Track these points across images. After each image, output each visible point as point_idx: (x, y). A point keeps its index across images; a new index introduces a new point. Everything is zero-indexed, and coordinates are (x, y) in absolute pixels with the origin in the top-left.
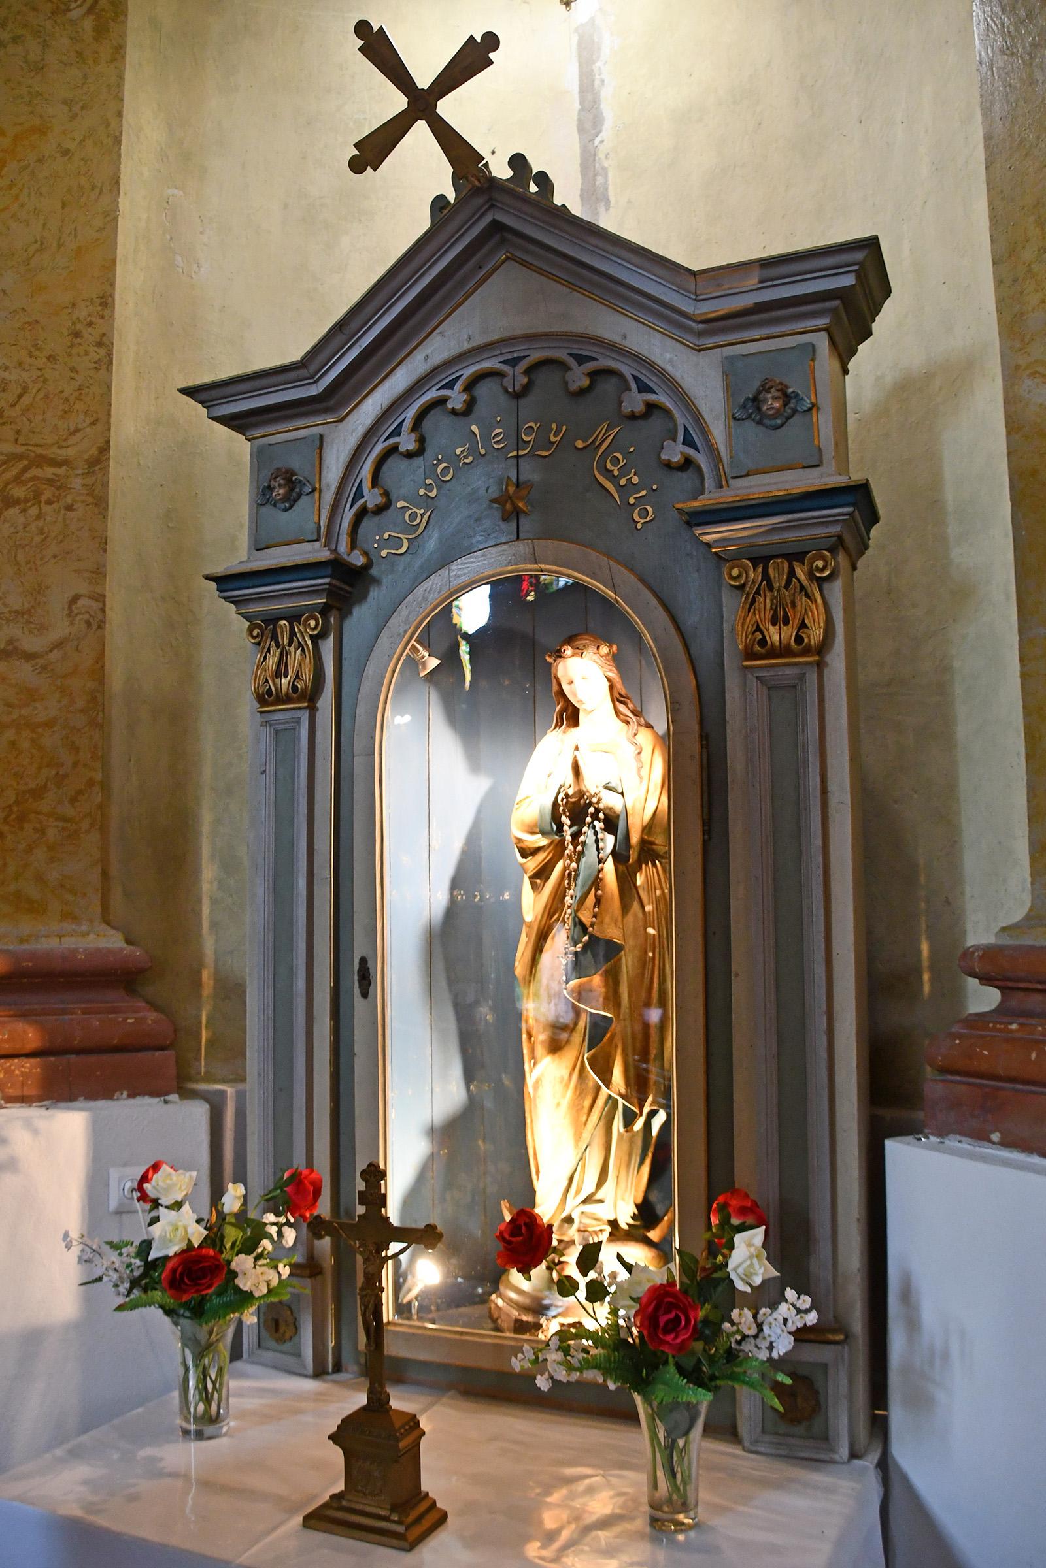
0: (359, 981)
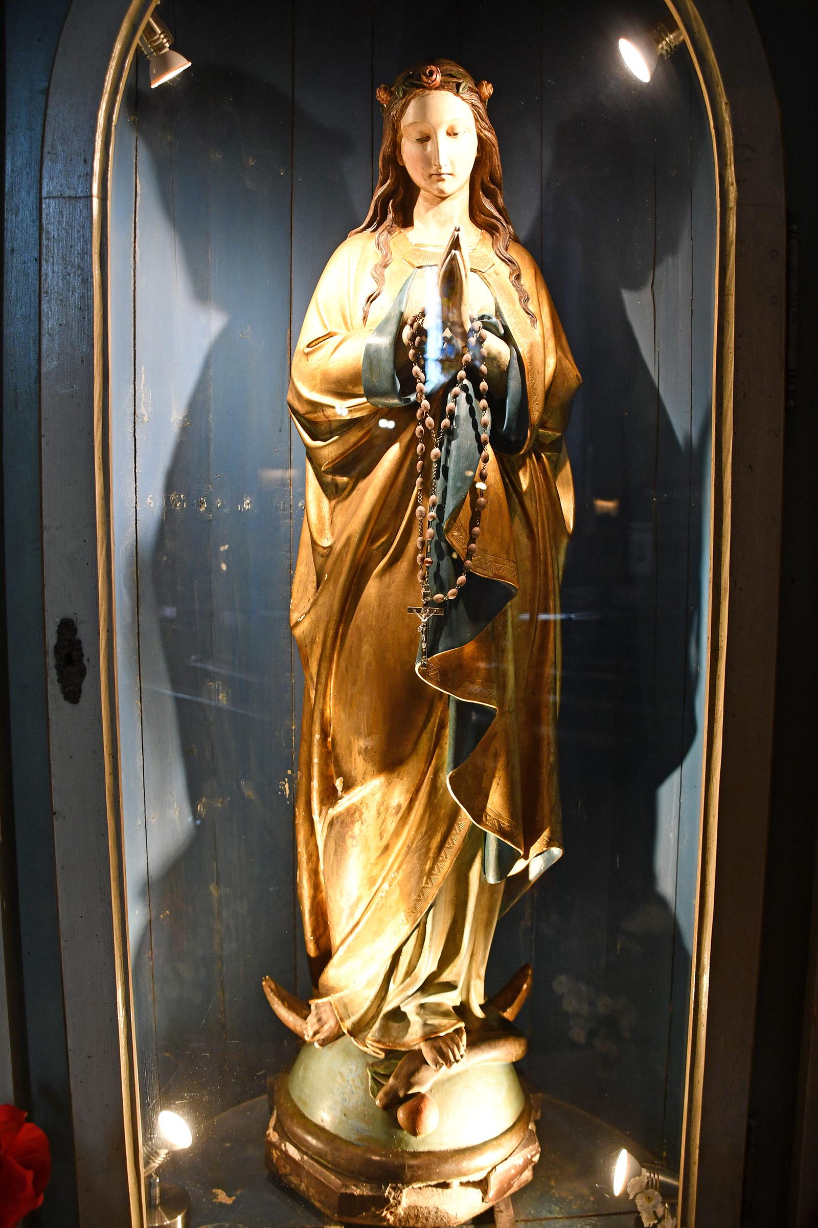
0: (58, 667)
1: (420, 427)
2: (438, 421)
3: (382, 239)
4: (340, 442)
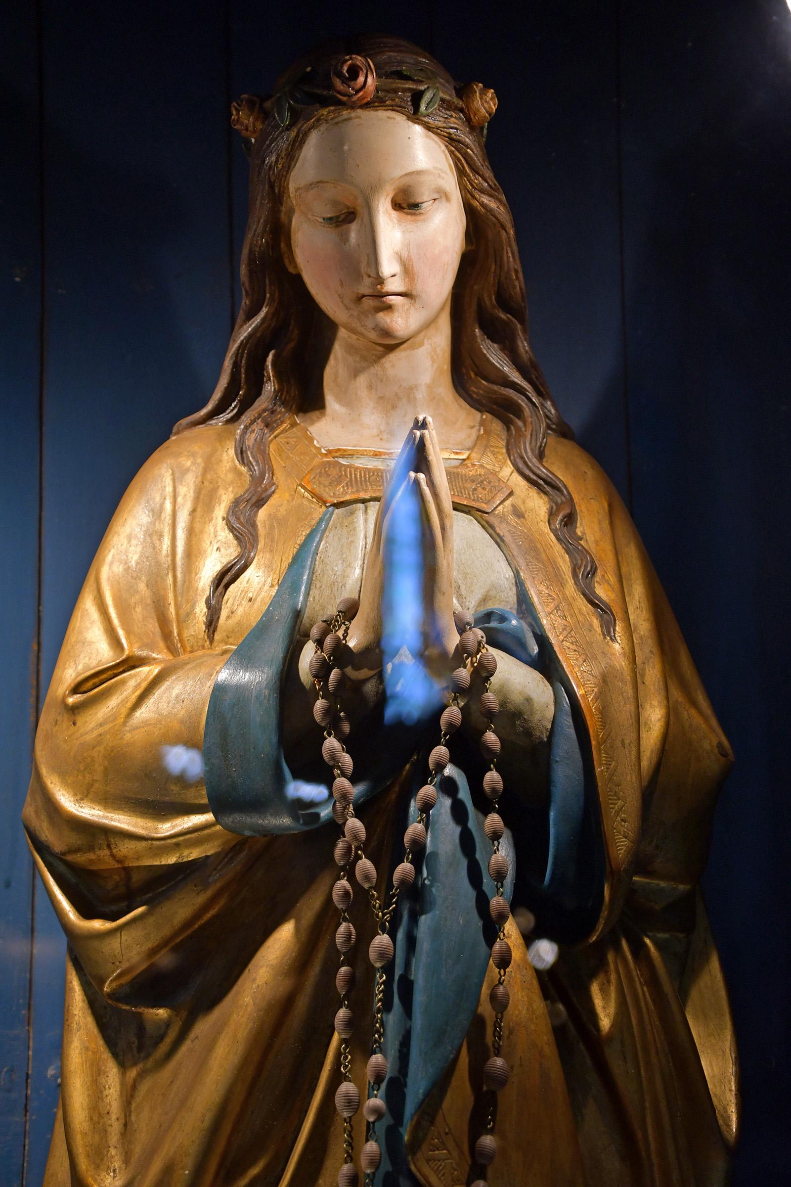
1: (344, 882)
2: (385, 866)
3: (251, 439)
4: (151, 920)
